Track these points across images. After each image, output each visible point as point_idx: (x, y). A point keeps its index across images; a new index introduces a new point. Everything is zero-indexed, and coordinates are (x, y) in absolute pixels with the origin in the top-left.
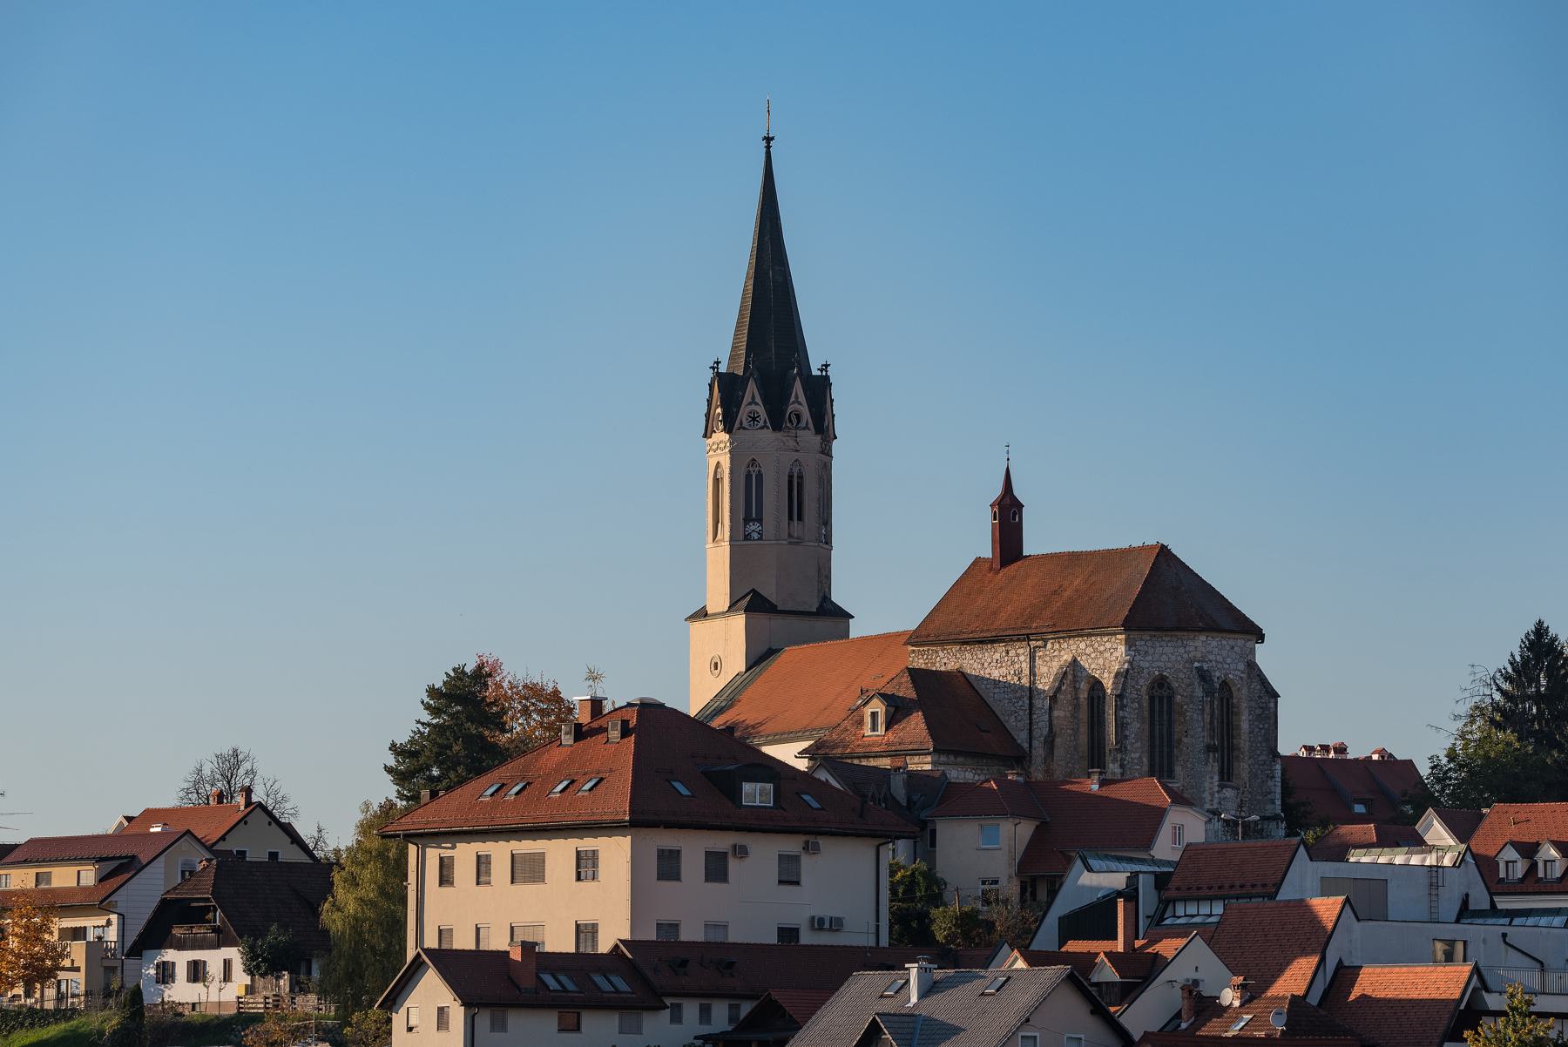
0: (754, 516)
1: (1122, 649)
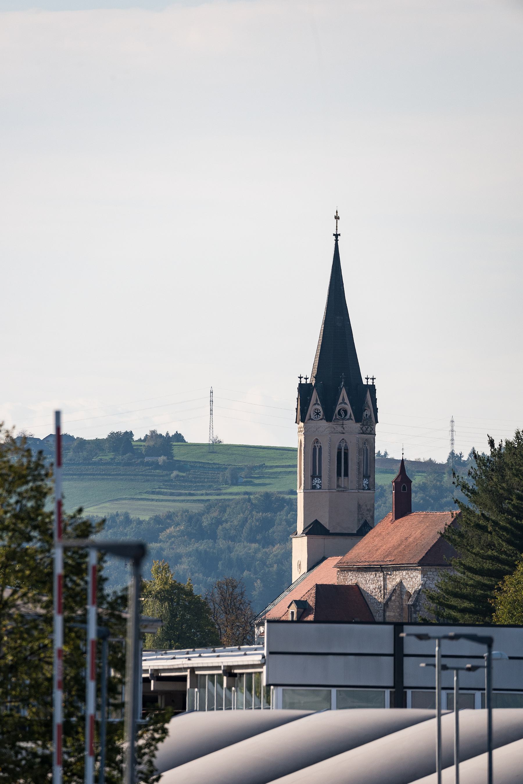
1: (420, 576)
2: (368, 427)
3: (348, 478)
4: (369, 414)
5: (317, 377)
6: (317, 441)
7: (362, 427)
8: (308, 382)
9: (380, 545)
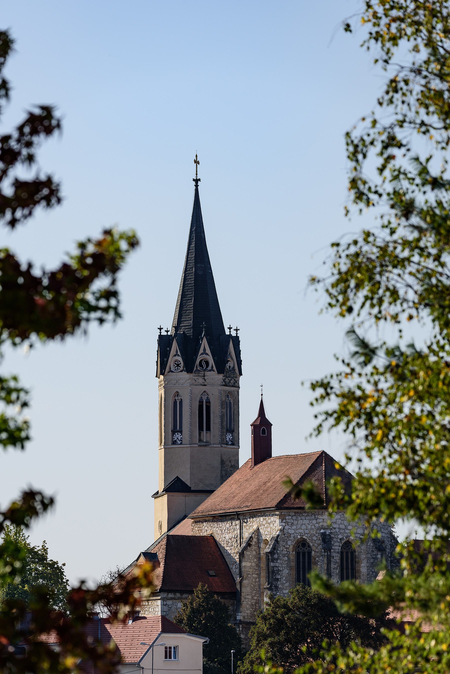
0: (178, 429)
3: (210, 433)
4: (232, 366)
5: (177, 328)
8: (169, 333)
9: (238, 492)
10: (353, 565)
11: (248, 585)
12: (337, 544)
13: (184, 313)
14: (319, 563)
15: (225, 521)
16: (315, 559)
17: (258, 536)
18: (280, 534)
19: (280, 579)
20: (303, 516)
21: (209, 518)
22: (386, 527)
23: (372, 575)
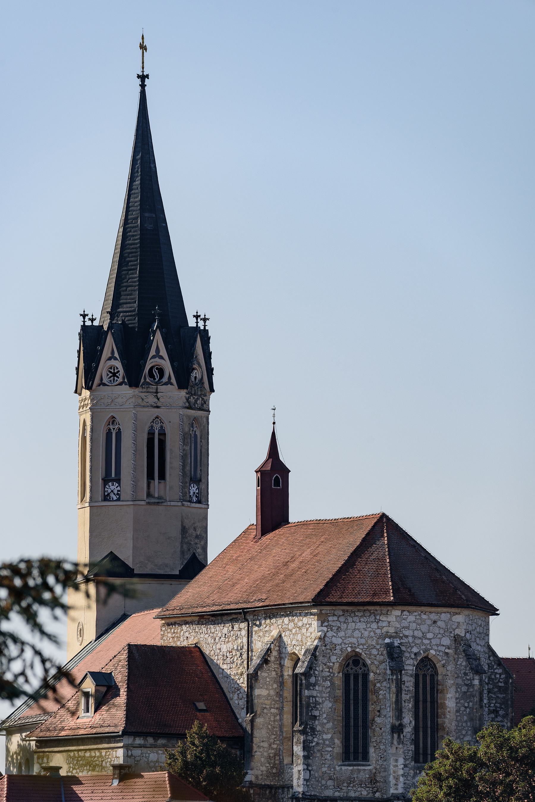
0: (113, 475)
2: (198, 399)
3: (165, 483)
4: (199, 377)
5: (113, 314)
6: (113, 420)
7: (189, 398)
8: (96, 323)
9: (238, 577)
10: (434, 696)
11: (263, 725)
12: (410, 662)
13: (123, 291)
14: (381, 692)
15: (221, 624)
16: (375, 686)
17: (279, 647)
18: (319, 644)
19: (319, 716)
20: (355, 616)
21: (193, 618)
22: (483, 635)
23: (465, 713)
